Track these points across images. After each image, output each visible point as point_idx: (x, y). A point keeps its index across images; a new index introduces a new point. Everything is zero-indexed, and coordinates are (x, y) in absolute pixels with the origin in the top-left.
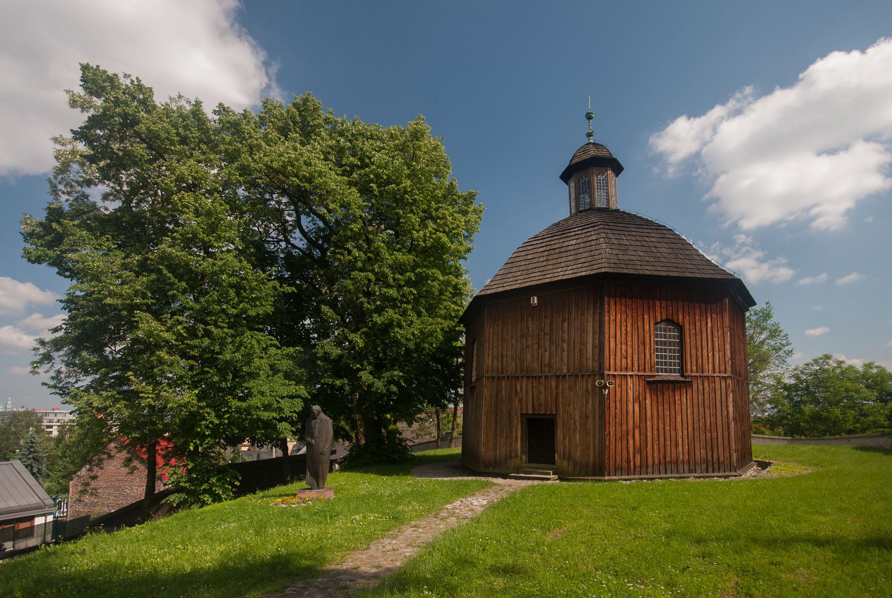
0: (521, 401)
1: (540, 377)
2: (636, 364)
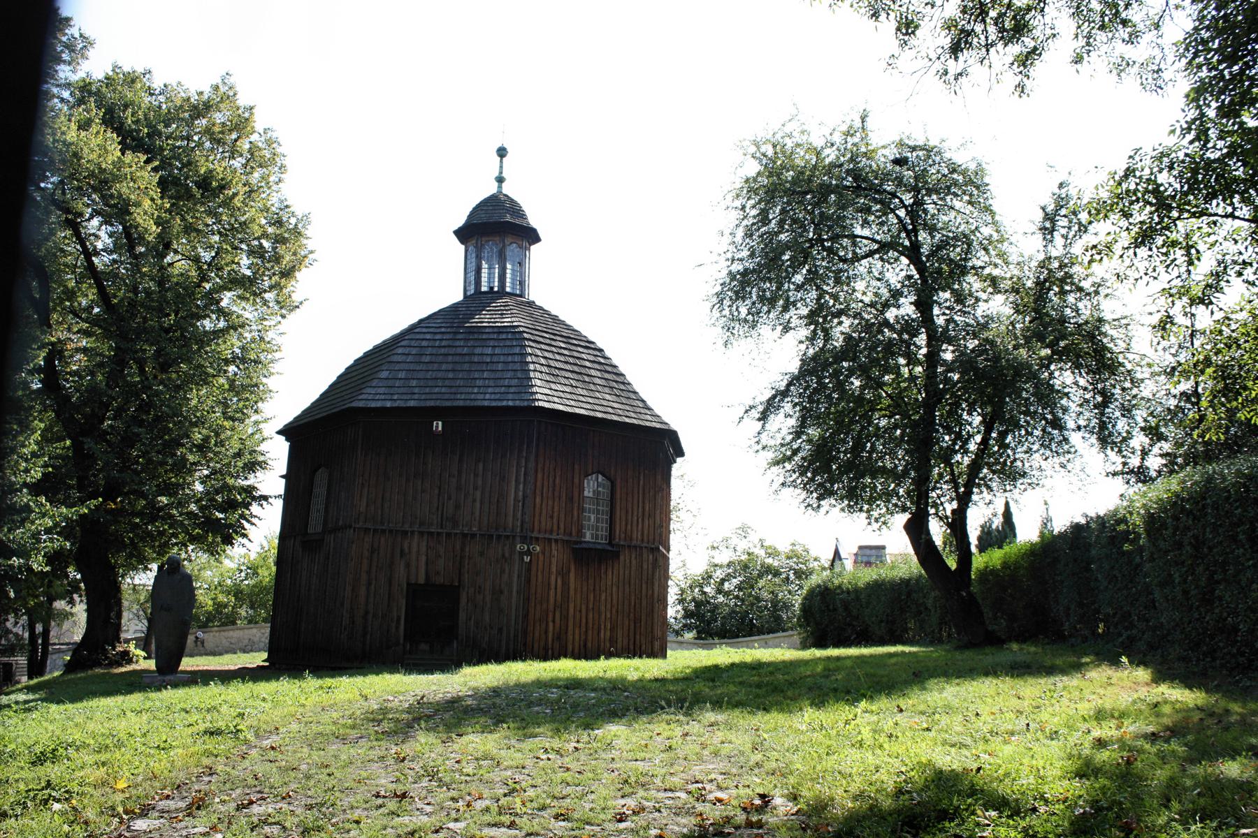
0: (408, 565)
1: (439, 534)
2: (562, 526)
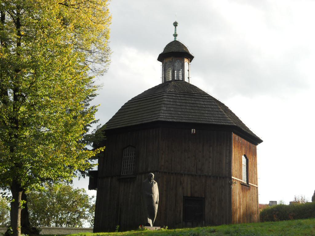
0: (183, 188)
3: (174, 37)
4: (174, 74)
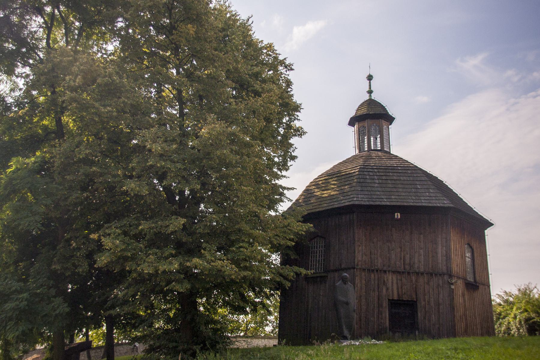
0: (387, 289)
3: (368, 95)
4: (363, 142)
